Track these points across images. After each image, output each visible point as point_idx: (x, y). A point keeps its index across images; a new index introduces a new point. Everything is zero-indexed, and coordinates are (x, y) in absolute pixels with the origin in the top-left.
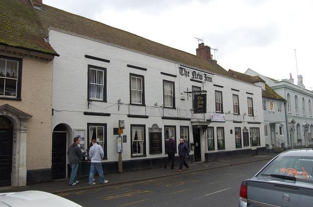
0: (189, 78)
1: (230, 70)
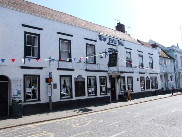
0: (106, 43)
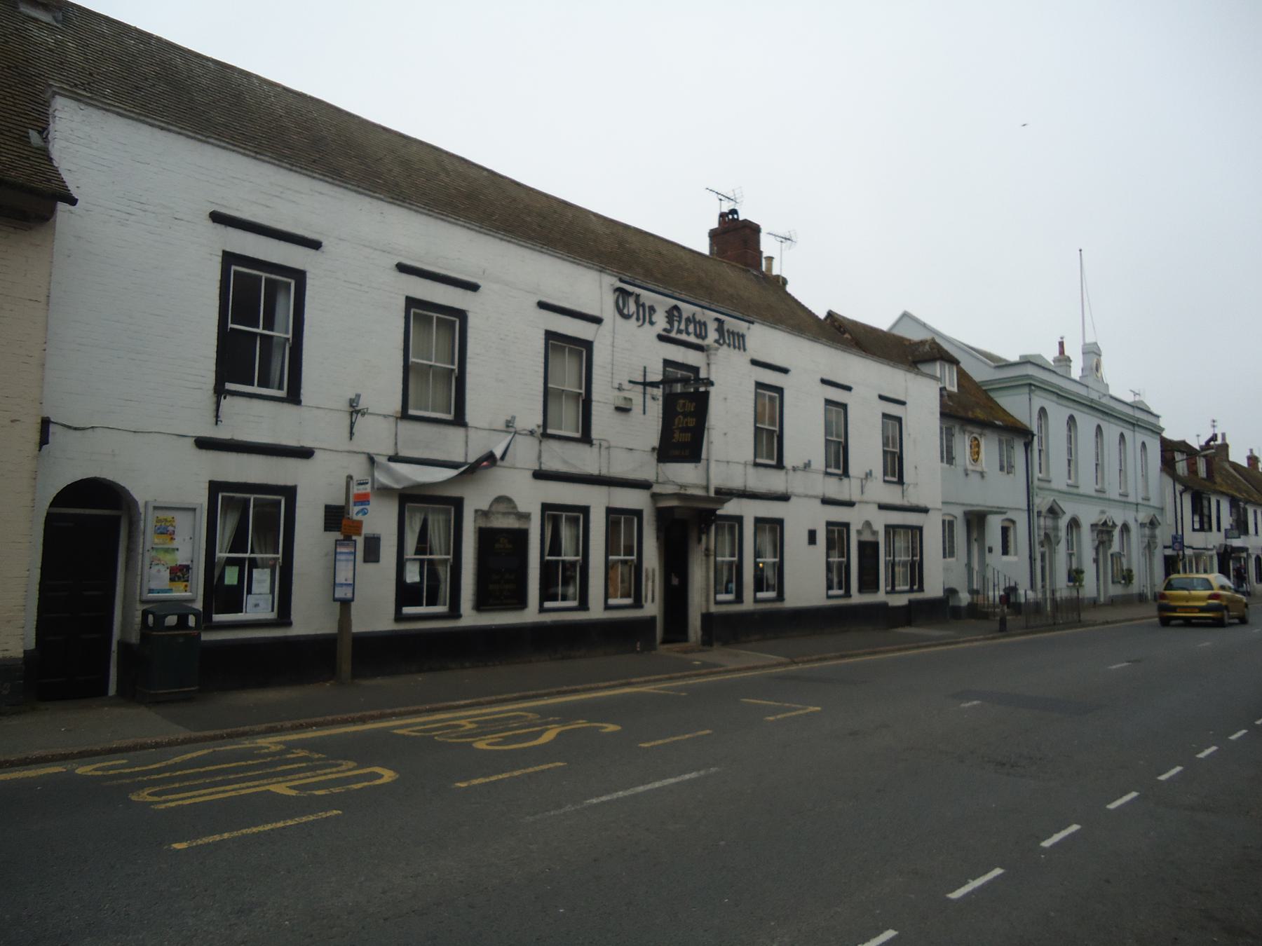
1: (830, 315)
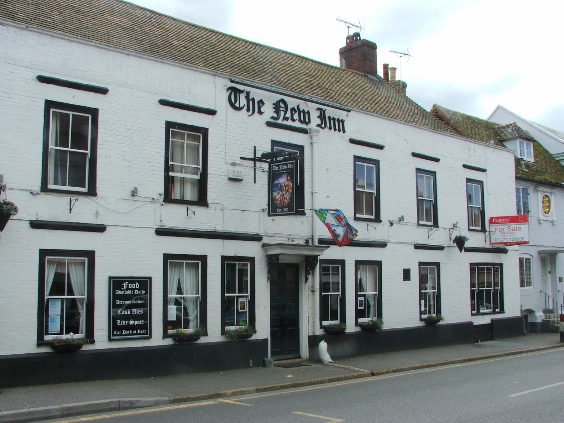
0: (259, 121)
